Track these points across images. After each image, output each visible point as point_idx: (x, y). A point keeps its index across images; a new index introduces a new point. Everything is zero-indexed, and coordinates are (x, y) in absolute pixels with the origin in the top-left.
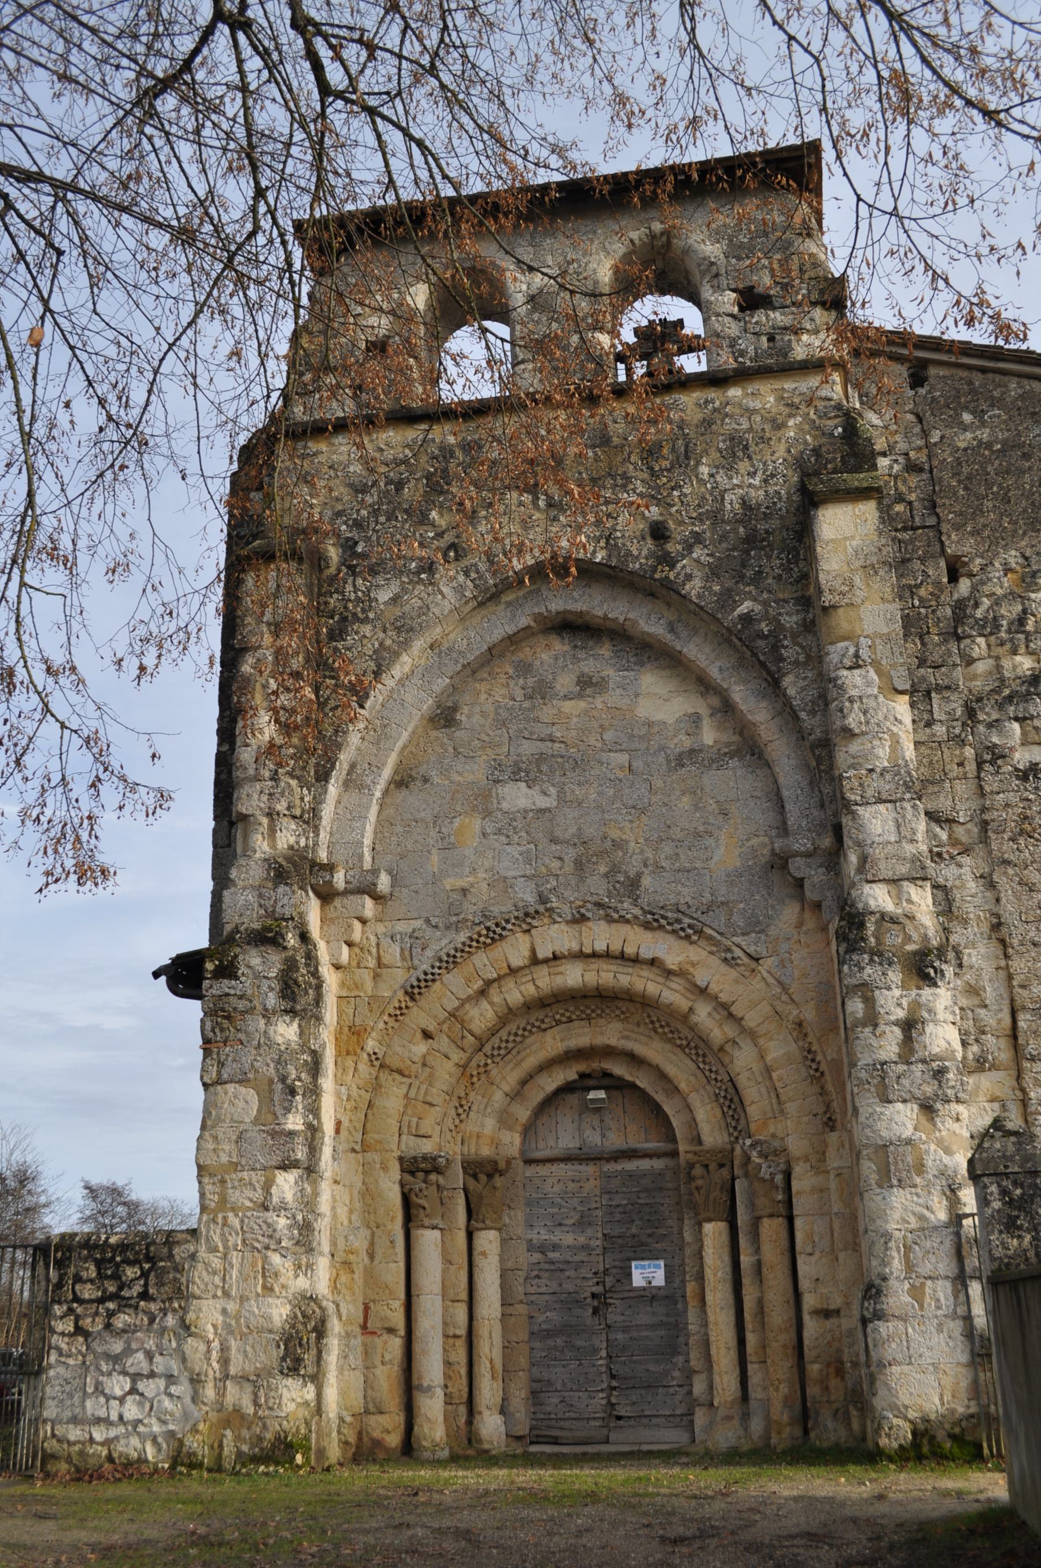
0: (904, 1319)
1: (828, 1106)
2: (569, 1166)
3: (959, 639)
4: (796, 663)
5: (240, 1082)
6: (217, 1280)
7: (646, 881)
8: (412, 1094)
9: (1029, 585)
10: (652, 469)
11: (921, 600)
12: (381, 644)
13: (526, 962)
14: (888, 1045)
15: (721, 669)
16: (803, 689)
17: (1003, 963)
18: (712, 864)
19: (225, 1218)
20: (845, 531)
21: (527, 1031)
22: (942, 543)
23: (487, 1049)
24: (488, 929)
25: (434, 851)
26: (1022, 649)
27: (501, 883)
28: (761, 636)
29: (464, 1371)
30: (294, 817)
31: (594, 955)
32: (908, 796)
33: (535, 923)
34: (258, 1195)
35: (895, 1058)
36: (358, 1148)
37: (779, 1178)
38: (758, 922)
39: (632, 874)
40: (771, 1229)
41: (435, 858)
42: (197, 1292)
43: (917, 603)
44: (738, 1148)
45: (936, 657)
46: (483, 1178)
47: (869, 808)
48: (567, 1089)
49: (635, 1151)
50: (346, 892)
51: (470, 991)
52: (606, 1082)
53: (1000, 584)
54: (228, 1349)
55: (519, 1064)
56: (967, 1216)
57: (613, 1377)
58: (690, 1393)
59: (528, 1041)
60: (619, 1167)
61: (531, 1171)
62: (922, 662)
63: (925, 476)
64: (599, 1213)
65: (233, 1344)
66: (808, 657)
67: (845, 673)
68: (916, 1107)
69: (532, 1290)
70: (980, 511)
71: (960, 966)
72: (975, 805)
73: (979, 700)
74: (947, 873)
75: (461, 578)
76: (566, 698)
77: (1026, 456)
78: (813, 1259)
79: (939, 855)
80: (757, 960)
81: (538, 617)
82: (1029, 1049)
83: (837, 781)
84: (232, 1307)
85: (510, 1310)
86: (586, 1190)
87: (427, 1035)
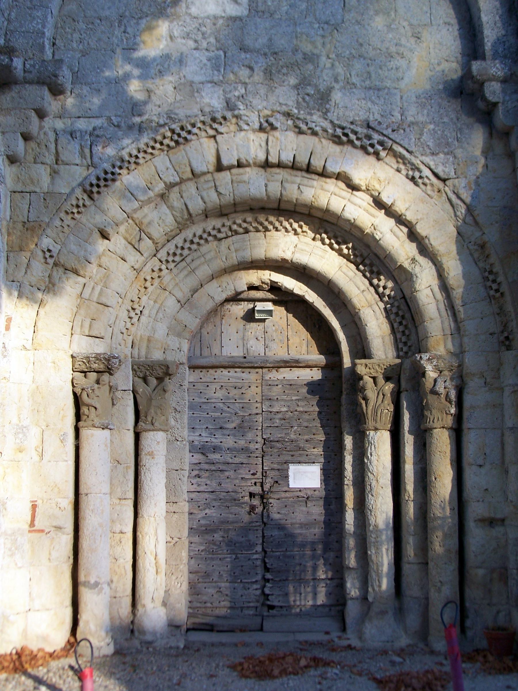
1: (505, 326)
7: (337, 96)
8: (86, 295)
13: (212, 168)
18: (402, 85)
21: (204, 238)
23: (162, 255)
24: (173, 131)
31: (280, 165)
33: (221, 129)
36: (29, 345)
39: (322, 88)
46: (153, 382)
49: (297, 361)
59: (204, 249)
60: (280, 377)
78: (483, 470)
80: (444, 181)
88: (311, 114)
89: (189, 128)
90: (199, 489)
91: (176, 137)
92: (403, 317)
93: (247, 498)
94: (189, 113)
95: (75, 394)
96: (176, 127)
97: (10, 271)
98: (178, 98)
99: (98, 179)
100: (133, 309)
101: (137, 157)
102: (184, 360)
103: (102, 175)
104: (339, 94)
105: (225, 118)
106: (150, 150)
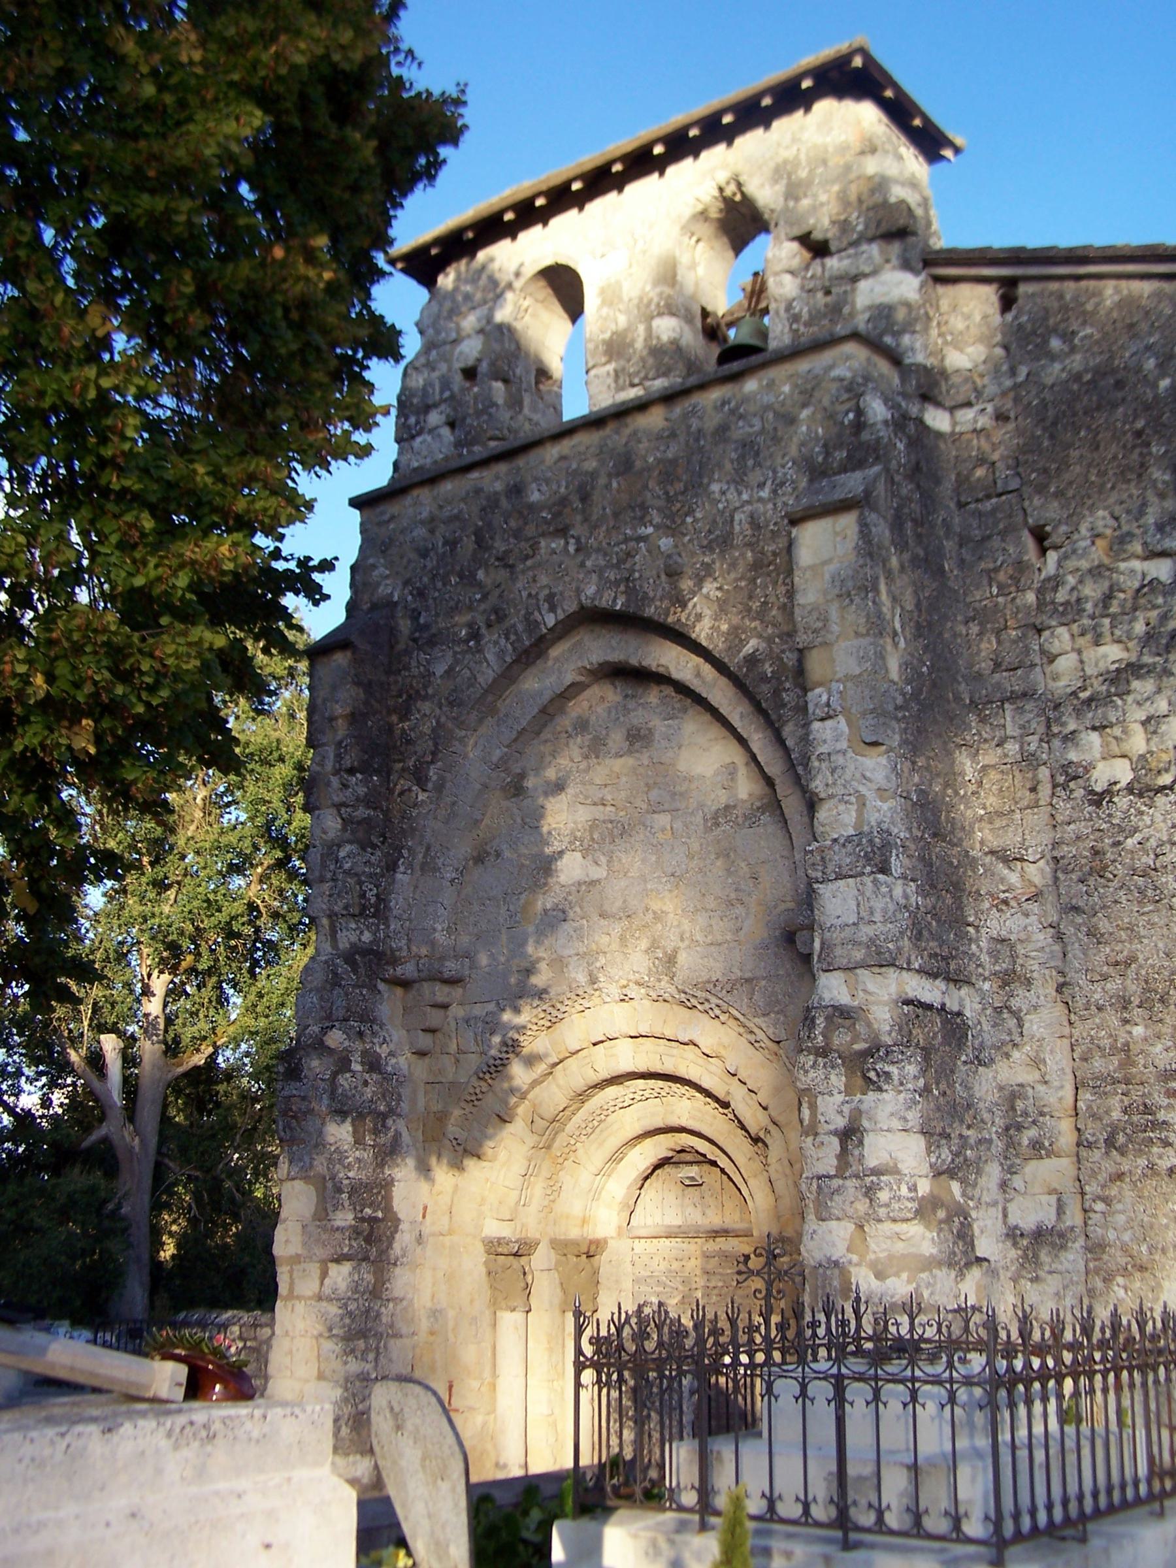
9: (1117, 553)
10: (667, 493)
12: (438, 722)
15: (742, 716)
17: (1067, 1031)
25: (504, 931)
26: (1108, 638)
28: (764, 679)
30: (354, 916)
32: (868, 869)
35: (833, 1173)
43: (995, 590)
47: (831, 886)
55: (601, 1145)
72: (1047, 838)
73: (1057, 706)
75: (503, 641)
77: (1119, 385)
81: (583, 670)
86: (688, 1269)
88: (659, 980)
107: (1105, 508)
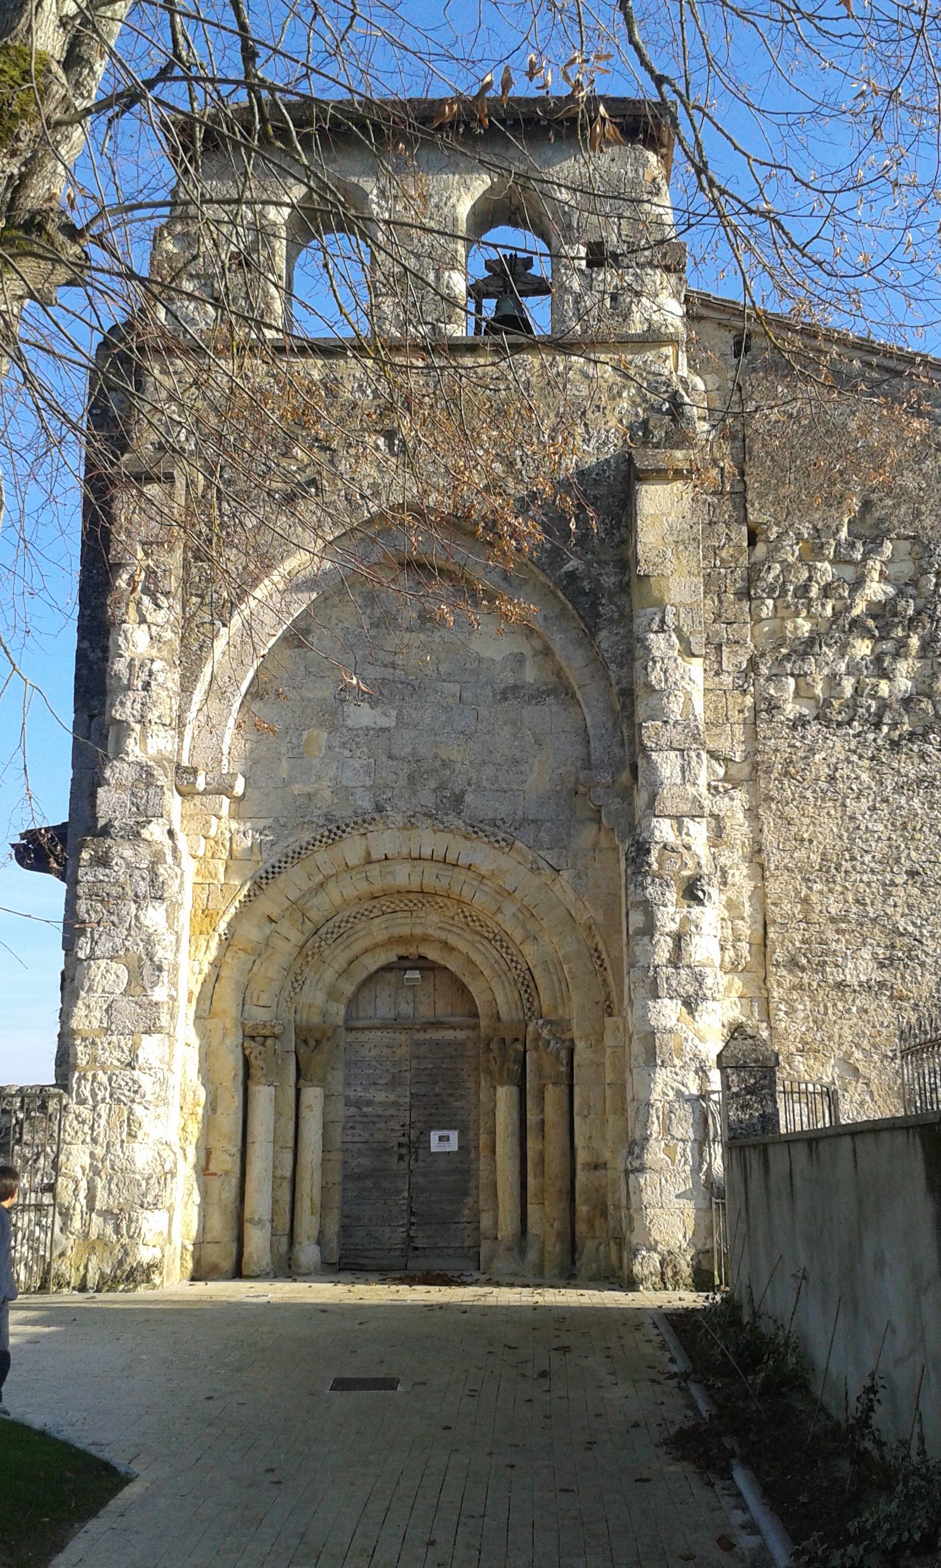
0: (659, 1172)
1: (608, 995)
2: (385, 1034)
3: (750, 599)
4: (611, 620)
5: (111, 958)
6: (86, 1128)
7: (469, 798)
9: (817, 555)
11: (722, 560)
14: (663, 952)
16: (616, 643)
18: (526, 787)
19: (94, 1076)
20: (661, 508)
22: (746, 509)
24: (330, 831)
25: (284, 759)
27: (342, 791)
29: (287, 1208)
32: (694, 746)
34: (126, 1057)
37: (563, 1054)
38: (562, 840)
40: (553, 1094)
41: (285, 764)
42: (68, 1139)
43: (718, 563)
44: (530, 1028)
45: (730, 615)
48: (387, 968)
50: (205, 793)
51: (311, 884)
52: (421, 963)
53: (791, 553)
54: (95, 1187)
56: (714, 1092)
57: (412, 1214)
58: (478, 1228)
60: (428, 1037)
61: (351, 1037)
62: (718, 617)
63: (738, 444)
64: (408, 1075)
65: (100, 1183)
66: (622, 615)
67: (652, 636)
68: (680, 1002)
69: (348, 1139)
70: (781, 482)
71: (725, 884)
74: (722, 805)
76: (409, 630)
79: (716, 788)
82: (775, 956)
83: (635, 728)
84: (100, 1151)
85: (329, 1156)
87: (271, 920)
89: (344, 827)
90: (354, 1140)
91: (332, 836)
92: (528, 986)
93: (396, 1148)
94: (344, 814)
95: (244, 1055)
96: (332, 827)
97: (192, 952)
98: (336, 801)
99: (267, 872)
100: (297, 981)
101: (299, 853)
102: (341, 1023)
103: (270, 870)
104: (472, 797)
105: (373, 819)
106: (311, 847)
107: (810, 522)
